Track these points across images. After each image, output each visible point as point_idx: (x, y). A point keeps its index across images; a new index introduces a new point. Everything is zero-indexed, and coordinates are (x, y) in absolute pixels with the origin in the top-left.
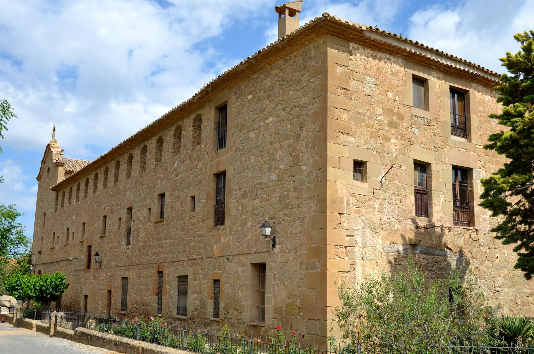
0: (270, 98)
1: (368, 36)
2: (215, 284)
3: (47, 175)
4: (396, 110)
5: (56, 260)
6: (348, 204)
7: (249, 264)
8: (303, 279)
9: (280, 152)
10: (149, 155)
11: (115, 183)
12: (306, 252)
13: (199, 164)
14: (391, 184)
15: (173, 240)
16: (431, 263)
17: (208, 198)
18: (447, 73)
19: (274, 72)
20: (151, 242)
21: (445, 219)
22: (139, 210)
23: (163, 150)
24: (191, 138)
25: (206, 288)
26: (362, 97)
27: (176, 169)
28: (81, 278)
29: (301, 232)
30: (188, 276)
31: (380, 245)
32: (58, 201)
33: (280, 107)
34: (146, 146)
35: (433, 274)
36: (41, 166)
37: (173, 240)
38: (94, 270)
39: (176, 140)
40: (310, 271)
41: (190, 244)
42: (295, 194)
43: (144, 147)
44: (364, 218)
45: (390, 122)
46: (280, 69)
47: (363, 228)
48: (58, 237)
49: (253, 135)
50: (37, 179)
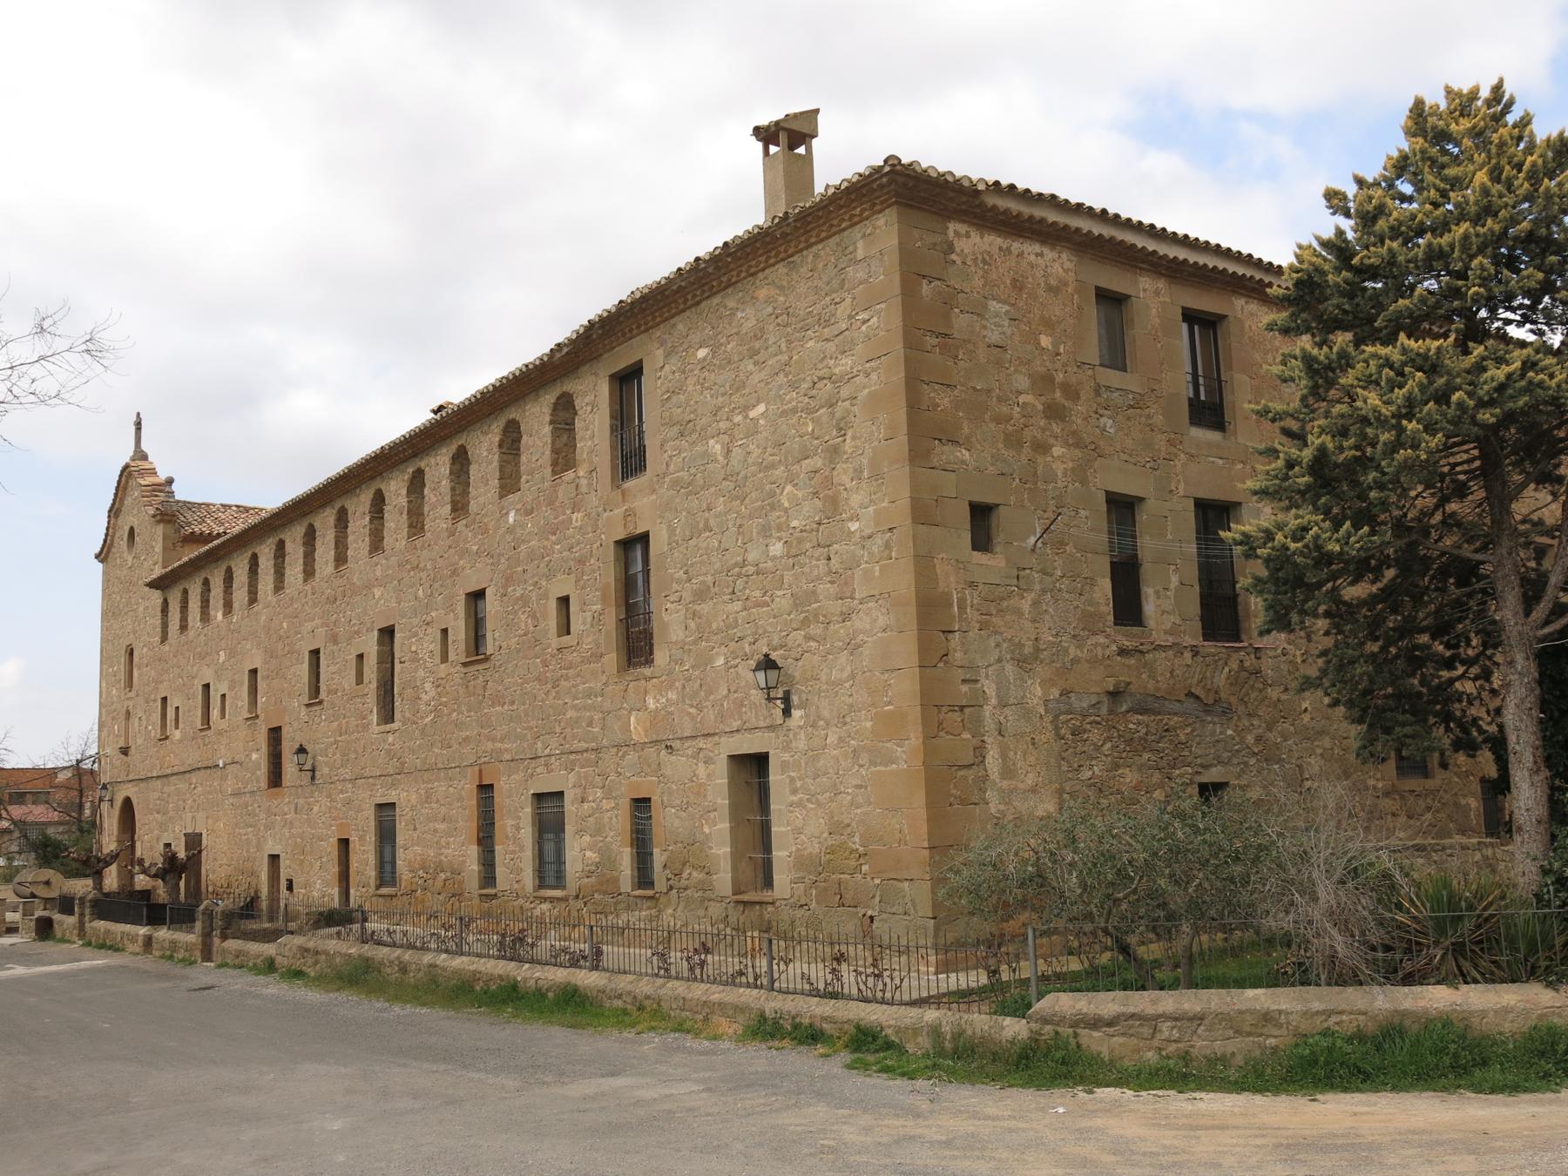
0: (756, 357)
1: (991, 204)
2: (637, 809)
3: (128, 546)
4: (1060, 377)
5: (176, 769)
6: (962, 607)
7: (724, 757)
8: (866, 787)
9: (789, 488)
10: (432, 496)
11: (336, 567)
12: (869, 724)
13: (574, 517)
14: (1057, 554)
15: (515, 707)
16: (1154, 731)
17: (604, 600)
18: (1176, 278)
19: (762, 293)
20: (455, 714)
21: (1182, 628)
22: (416, 635)
23: (471, 481)
24: (548, 452)
25: (614, 819)
26: (982, 354)
27: (511, 530)
28: (257, 811)
29: (853, 676)
30: (563, 792)
31: (1039, 698)
32: (170, 614)
33: (781, 378)
34: (420, 473)
35: (1162, 758)
36: (109, 523)
37: (515, 707)
38: (293, 790)
39: (505, 457)
40: (883, 768)
41: (564, 714)
42: (833, 589)
43: (416, 474)
44: (999, 638)
45: (1049, 407)
46: (778, 287)
47: (999, 660)
48: (177, 708)
49: (716, 447)
50: (97, 557)
